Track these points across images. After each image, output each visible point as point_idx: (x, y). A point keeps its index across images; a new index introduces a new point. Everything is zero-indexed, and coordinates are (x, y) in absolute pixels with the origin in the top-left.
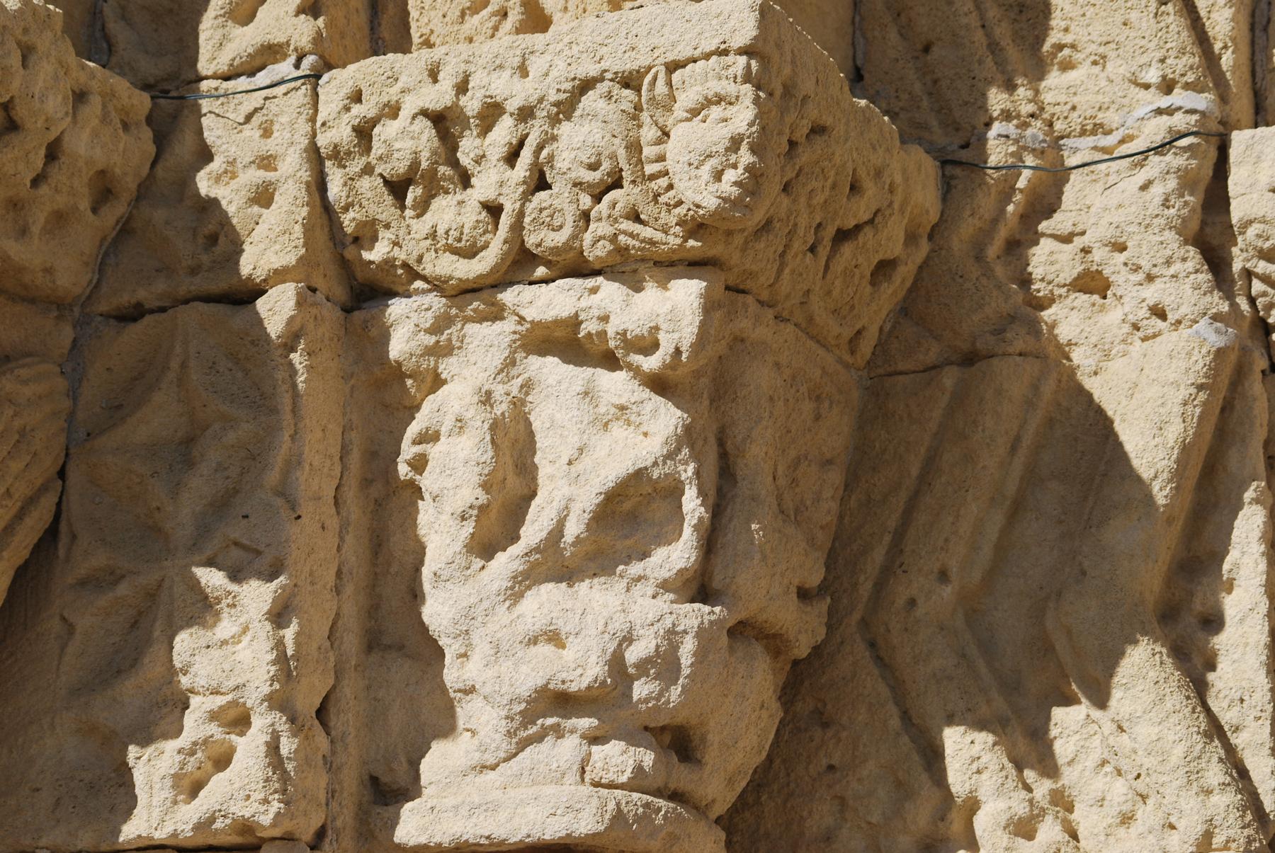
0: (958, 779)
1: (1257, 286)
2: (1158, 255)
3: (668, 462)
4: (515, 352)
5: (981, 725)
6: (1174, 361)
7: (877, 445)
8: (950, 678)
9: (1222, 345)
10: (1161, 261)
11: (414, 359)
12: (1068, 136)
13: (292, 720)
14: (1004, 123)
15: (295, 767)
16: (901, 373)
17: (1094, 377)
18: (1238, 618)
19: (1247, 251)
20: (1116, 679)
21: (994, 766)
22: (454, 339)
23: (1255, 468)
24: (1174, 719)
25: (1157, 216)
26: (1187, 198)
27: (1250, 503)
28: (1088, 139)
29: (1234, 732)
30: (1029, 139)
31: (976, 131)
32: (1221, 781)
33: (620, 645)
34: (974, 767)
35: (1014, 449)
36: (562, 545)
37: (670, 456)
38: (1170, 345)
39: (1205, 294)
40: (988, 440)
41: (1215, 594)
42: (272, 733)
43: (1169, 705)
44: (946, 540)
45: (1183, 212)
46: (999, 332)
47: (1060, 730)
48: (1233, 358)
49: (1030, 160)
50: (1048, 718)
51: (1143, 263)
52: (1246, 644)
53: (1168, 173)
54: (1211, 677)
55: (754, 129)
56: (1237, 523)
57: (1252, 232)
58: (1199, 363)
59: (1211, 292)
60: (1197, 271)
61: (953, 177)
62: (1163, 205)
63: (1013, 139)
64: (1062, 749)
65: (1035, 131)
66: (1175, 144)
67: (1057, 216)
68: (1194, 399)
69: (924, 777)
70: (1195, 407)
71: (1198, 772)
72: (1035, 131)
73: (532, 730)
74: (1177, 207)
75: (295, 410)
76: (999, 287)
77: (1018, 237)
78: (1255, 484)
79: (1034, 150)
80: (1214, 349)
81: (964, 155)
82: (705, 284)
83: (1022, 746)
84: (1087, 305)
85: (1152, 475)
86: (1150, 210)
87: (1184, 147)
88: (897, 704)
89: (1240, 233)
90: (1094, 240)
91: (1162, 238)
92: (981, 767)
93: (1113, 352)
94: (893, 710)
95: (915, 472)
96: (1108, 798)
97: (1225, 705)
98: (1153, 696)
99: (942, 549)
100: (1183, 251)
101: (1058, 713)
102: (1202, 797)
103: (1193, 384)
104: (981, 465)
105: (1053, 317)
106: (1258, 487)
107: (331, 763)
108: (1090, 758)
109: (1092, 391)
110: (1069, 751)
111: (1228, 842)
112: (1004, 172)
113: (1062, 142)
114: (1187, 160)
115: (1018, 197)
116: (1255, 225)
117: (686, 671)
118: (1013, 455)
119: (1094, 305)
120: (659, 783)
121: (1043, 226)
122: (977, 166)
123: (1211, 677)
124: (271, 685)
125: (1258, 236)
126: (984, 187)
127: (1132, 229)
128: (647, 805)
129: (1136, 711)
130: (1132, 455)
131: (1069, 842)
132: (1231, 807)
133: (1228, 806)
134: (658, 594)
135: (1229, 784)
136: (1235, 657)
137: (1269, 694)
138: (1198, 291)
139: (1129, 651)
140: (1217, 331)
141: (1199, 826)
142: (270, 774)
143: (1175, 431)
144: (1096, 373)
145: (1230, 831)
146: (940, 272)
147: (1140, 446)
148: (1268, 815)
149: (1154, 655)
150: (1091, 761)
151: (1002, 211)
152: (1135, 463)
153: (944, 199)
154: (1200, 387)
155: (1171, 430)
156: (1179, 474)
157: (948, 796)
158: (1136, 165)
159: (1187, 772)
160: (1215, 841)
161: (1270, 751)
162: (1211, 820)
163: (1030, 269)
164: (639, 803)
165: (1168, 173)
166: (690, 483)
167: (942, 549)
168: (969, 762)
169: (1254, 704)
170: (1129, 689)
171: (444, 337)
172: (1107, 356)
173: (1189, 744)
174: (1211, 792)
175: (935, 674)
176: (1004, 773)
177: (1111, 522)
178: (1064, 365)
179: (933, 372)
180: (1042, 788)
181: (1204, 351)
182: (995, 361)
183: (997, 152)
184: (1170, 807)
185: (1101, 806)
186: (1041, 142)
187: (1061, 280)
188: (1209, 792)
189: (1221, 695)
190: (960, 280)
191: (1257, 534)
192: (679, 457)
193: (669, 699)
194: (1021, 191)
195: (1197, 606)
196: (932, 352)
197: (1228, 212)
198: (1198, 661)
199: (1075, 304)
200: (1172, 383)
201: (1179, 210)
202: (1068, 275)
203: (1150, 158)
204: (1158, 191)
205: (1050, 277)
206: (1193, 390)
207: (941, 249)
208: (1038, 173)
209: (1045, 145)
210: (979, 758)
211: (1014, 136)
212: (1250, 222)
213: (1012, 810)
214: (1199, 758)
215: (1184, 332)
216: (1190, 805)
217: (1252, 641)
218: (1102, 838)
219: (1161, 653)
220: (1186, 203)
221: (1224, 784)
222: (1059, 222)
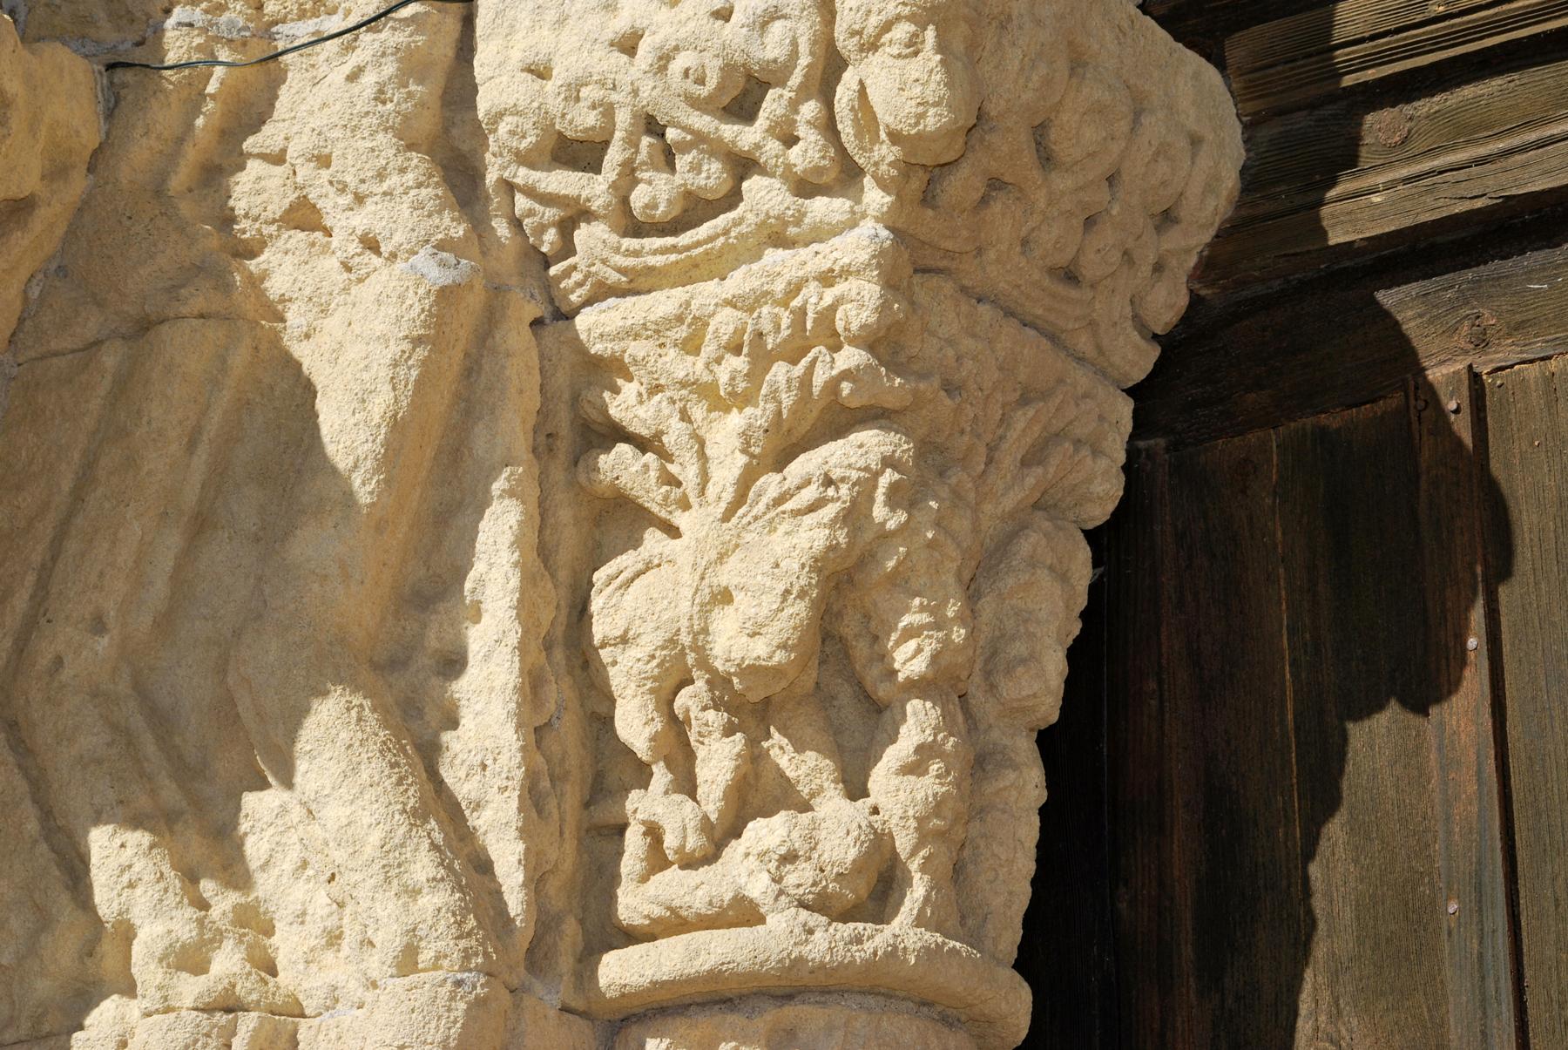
0: (105, 899)
1: (522, 203)
2: (367, 166)
5: (136, 822)
6: (382, 308)
7: (24, 454)
8: (99, 762)
9: (450, 281)
10: (370, 174)
12: (284, 21)
14: (188, 7)
16: (55, 354)
17: (305, 342)
18: (482, 654)
19: (501, 155)
20: (299, 746)
21: (149, 877)
23: (509, 449)
24: (370, 794)
25: (367, 113)
26: (412, 87)
27: (501, 496)
28: (310, 22)
29: (474, 810)
30: (223, 27)
31: (151, 21)
32: (431, 876)
34: (125, 879)
35: (191, 446)
38: (378, 287)
39: (429, 216)
40: (154, 436)
41: (455, 623)
43: (365, 776)
44: (101, 574)
45: (404, 106)
46: (173, 290)
47: (251, 823)
48: (475, 300)
49: (224, 55)
50: (238, 808)
51: (348, 178)
52: (492, 689)
53: (384, 54)
54: (447, 737)
56: (482, 525)
57: (503, 128)
58: (415, 307)
59: (440, 212)
60: (419, 185)
61: (124, 85)
62: (376, 99)
64: (255, 849)
65: (233, 15)
66: (393, 15)
67: (267, 129)
68: (409, 358)
69: (65, 898)
70: (409, 369)
71: (399, 865)
72: (233, 15)
74: (395, 100)
76: (181, 230)
77: (217, 161)
78: (507, 472)
79: (231, 41)
80: (437, 287)
81: (138, 55)
83: (196, 847)
84: (302, 245)
85: (351, 464)
86: (358, 107)
87: (406, 19)
88: (35, 801)
89: (490, 133)
90: (295, 155)
91: (374, 143)
92: (134, 878)
93: (333, 306)
94: (29, 810)
95: (67, 485)
96: (310, 911)
97: (462, 774)
98: (343, 765)
99: (95, 587)
100: (400, 159)
101: (250, 800)
102: (404, 898)
103: (407, 337)
104: (146, 469)
105: (263, 266)
106: (512, 474)
108: (288, 859)
109: (302, 360)
110: (262, 851)
111: (437, 958)
112: (187, 72)
113: (274, 29)
114: (410, 36)
115: (210, 106)
116: (508, 119)
118: (192, 454)
119: (313, 244)
121: (250, 144)
122: (153, 67)
123: (447, 737)
125: (512, 133)
126: (161, 96)
127: (337, 133)
129: (324, 787)
130: (326, 439)
131: (249, 974)
132: (444, 910)
133: (439, 910)
135: (442, 879)
136: (478, 707)
137: (519, 755)
138: (418, 212)
139: (315, 707)
140: (443, 264)
141: (398, 939)
143: (381, 403)
144: (307, 336)
145: (439, 944)
146: (104, 214)
147: (336, 426)
148: (513, 920)
149: (348, 709)
150: (288, 864)
151: (190, 126)
152: (330, 449)
153: (110, 115)
154: (417, 341)
155: (377, 401)
156: (392, 457)
157: (98, 922)
158: (347, 49)
159: (384, 866)
160: (421, 958)
161: (517, 833)
162: (414, 930)
163: (231, 203)
165: (384, 54)
167: (95, 587)
168: (117, 872)
169: (498, 770)
170: (315, 758)
172: (325, 312)
173: (388, 828)
174: (420, 891)
175: (81, 757)
176: (162, 885)
177: (298, 532)
178: (263, 327)
179: (94, 349)
180: (223, 903)
181: (421, 291)
182: (165, 328)
183: (177, 45)
184: (365, 915)
185: (302, 923)
186: (239, 30)
187: (269, 215)
188: (415, 893)
189: (457, 762)
190: (128, 223)
191: (508, 537)
194: (213, 97)
195: (432, 642)
196: (91, 324)
197: (474, 108)
198: (432, 716)
199: (288, 246)
200: (379, 338)
201: (398, 104)
202: (277, 208)
203: (361, 36)
204: (369, 79)
205: (255, 212)
206: (406, 346)
207: (107, 183)
208: (236, 71)
209: (247, 34)
210: (130, 866)
212: (500, 115)
213: (173, 934)
214: (403, 845)
215: (400, 265)
216: (388, 911)
217: (498, 684)
218: (301, 967)
219: (361, 706)
220: (410, 95)
221: (434, 879)
222: (267, 138)
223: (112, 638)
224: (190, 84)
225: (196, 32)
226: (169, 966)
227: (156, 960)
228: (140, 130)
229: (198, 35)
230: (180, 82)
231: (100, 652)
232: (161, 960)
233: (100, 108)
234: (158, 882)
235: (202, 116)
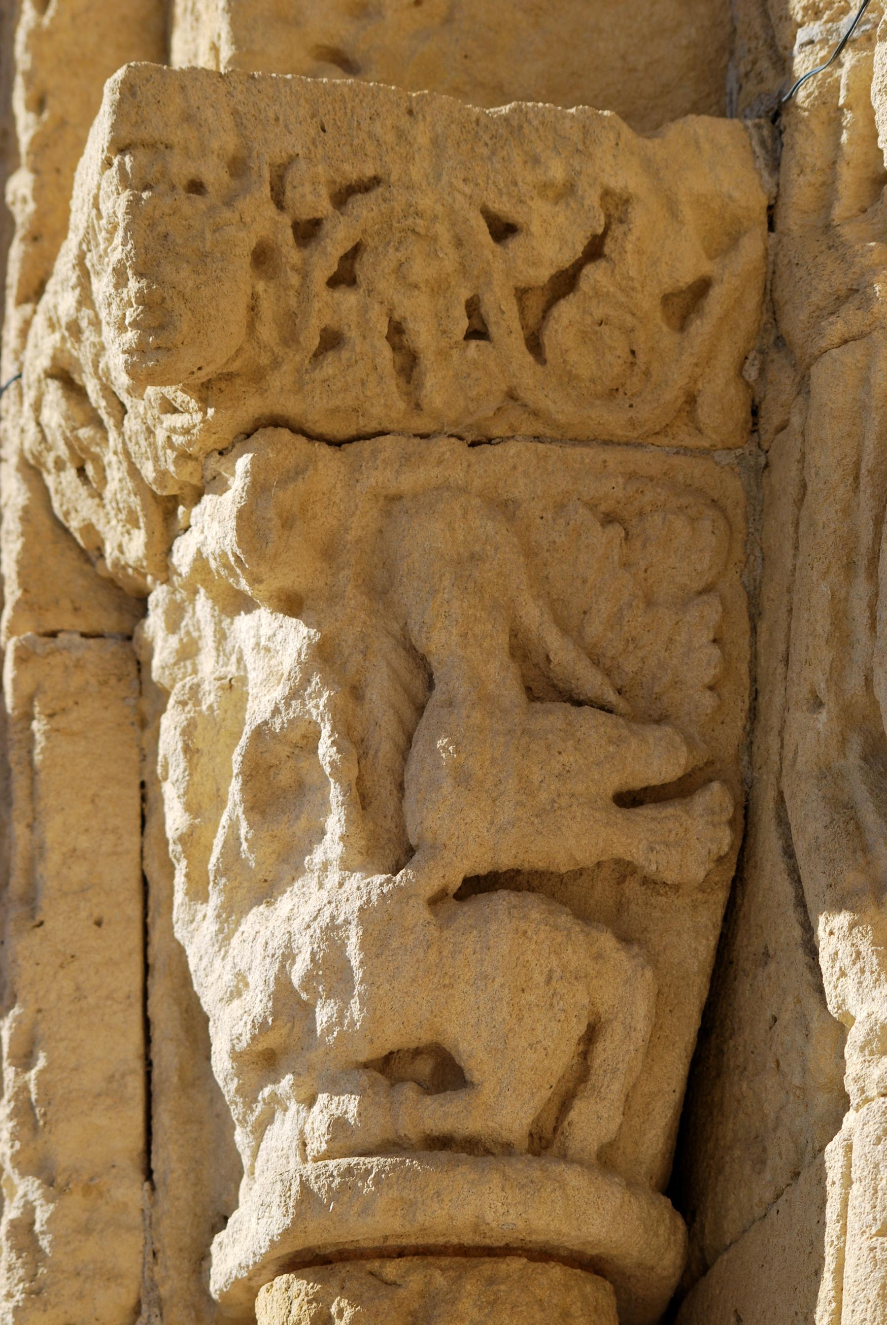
3: (293, 703)
4: (221, 621)
11: (167, 673)
13: (50, 1182)
15: (51, 1242)
22: (191, 629)
33: (283, 967)
36: (243, 856)
37: (295, 694)
42: (24, 1206)
55: (129, 246)
63: (820, 41)
73: (259, 1108)
75: (32, 795)
82: (250, 455)
107: (150, 1217)
117: (358, 975)
120: (377, 1133)
124: (12, 1147)
128: (349, 1171)
134: (344, 879)
142: (14, 1260)
151: (838, 146)
164: (335, 1173)
166: (323, 720)
171: (183, 631)
192: (309, 690)
193: (352, 1018)
194: (848, 106)
211: (819, 37)
223: (828, 712)
224: (824, 103)
225: (818, 47)
226: (872, 1053)
227: (858, 1050)
228: (795, 171)
229: (821, 49)
230: (813, 105)
231: (821, 730)
232: (862, 1049)
233: (760, 163)
234: (854, 964)
235: (844, 131)
